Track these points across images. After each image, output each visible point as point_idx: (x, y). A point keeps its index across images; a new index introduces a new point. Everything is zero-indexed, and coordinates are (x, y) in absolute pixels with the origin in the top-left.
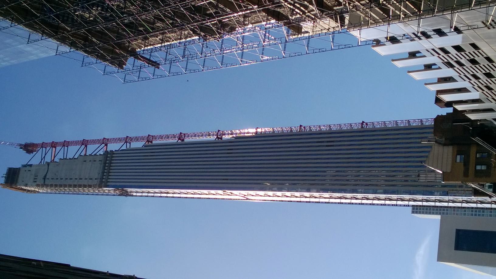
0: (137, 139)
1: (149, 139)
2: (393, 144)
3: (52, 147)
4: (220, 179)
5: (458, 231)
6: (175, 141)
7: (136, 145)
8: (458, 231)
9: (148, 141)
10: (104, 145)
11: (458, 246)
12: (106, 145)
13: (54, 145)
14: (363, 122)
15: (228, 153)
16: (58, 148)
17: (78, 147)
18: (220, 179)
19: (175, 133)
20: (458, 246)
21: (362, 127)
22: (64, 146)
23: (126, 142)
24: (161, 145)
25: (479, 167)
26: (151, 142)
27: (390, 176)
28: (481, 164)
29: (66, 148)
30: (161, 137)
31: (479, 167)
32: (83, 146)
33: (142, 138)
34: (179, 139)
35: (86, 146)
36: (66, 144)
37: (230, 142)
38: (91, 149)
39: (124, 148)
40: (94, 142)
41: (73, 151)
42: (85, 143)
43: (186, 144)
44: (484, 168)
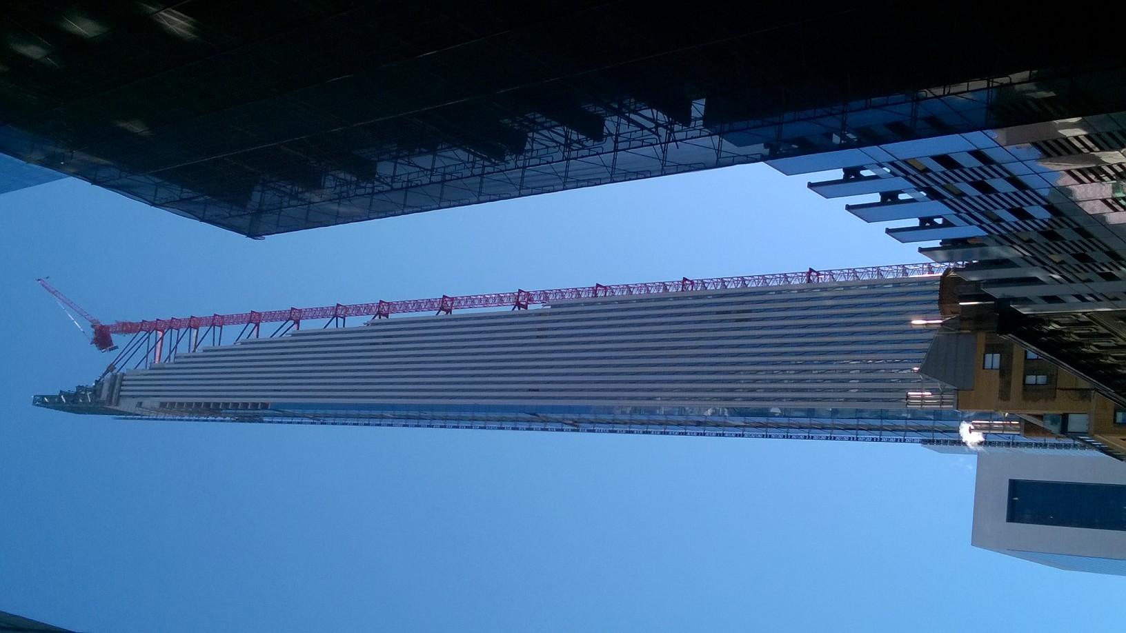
0: (358, 310)
1: (382, 309)
2: (671, 357)
3: (190, 327)
4: (627, 374)
5: (1015, 486)
6: (508, 309)
7: (355, 322)
8: (1015, 486)
9: (518, 304)
10: (291, 322)
11: (1014, 515)
12: (297, 322)
13: (193, 323)
14: (811, 270)
15: (538, 337)
16: (203, 330)
17: (242, 326)
18: (573, 382)
19: (325, 305)
20: (1014, 515)
21: (809, 281)
22: (213, 325)
23: (336, 316)
24: (491, 317)
25: (1031, 379)
26: (449, 311)
27: (867, 381)
28: (1036, 372)
29: (217, 329)
30: (405, 306)
31: (1031, 379)
32: (252, 325)
33: (367, 309)
34: (442, 309)
35: (257, 325)
36: (217, 321)
37: (540, 315)
38: (268, 330)
39: (332, 326)
40: (272, 317)
41: (230, 335)
42: (255, 319)
43: (456, 320)
44: (1041, 379)
